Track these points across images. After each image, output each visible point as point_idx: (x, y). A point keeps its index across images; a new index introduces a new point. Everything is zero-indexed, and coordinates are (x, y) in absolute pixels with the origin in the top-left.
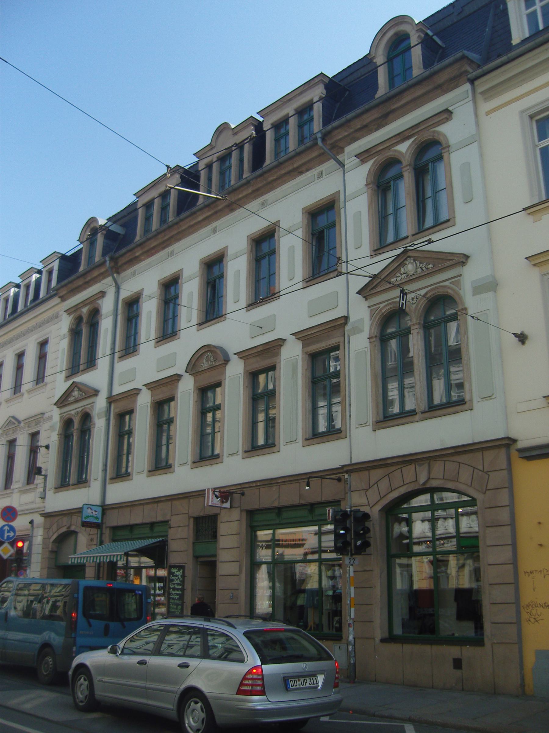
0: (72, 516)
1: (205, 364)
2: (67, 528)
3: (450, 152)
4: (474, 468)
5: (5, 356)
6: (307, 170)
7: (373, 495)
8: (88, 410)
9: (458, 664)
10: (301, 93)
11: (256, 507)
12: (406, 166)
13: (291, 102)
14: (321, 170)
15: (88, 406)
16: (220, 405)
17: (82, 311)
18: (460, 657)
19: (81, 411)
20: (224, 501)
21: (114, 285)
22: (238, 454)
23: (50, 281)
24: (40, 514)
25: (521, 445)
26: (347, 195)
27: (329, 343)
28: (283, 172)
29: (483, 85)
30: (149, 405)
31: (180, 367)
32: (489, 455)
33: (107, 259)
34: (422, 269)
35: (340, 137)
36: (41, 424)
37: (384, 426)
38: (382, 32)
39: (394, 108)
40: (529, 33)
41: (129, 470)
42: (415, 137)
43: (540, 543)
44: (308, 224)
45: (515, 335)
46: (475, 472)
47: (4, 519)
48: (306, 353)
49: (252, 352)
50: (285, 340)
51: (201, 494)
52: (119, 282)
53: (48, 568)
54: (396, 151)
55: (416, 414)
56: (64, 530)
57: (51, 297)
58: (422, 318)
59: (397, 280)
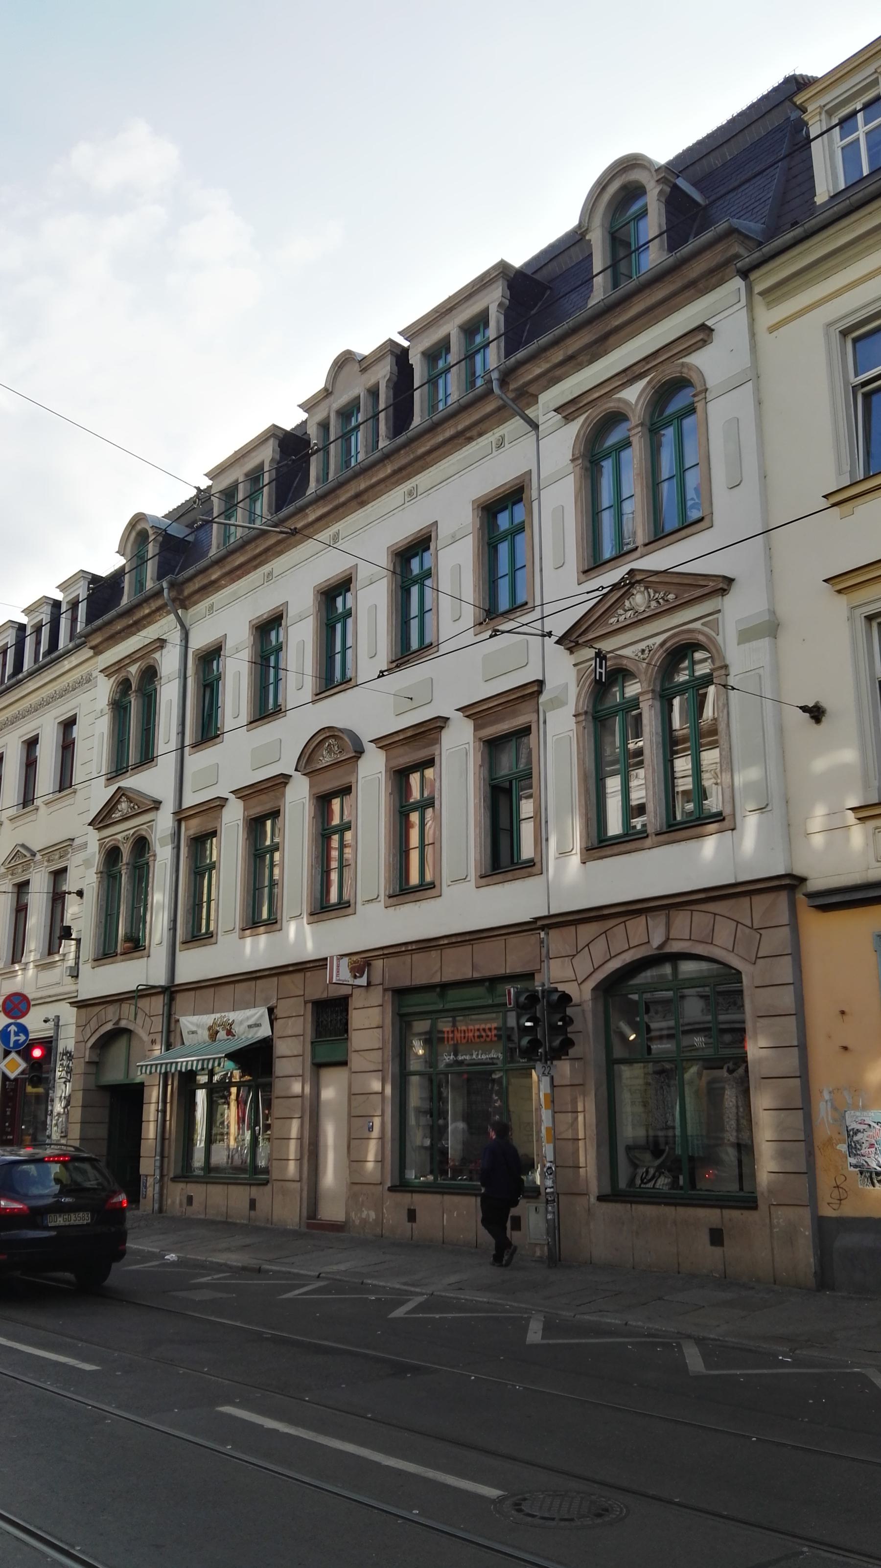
0: (121, 1005)
1: (325, 759)
2: (114, 1024)
3: (707, 400)
4: (738, 922)
5: (5, 745)
6: (480, 435)
7: (583, 966)
8: (144, 833)
9: (717, 1237)
11: (407, 983)
12: (637, 426)
13: (454, 312)
14: (501, 433)
15: (144, 827)
16: (350, 822)
17: (128, 672)
18: (719, 1227)
19: (133, 834)
21: (179, 627)
22: (378, 900)
23: (74, 620)
24: (70, 1003)
25: (814, 885)
26: (542, 477)
27: (515, 724)
28: (440, 438)
29: (764, 280)
30: (241, 823)
31: (287, 766)
32: (761, 902)
33: (165, 585)
34: (658, 602)
35: (530, 377)
36: (69, 856)
37: (598, 855)
38: (601, 186)
39: (617, 323)
40: (588, 566)
41: (212, 928)
42: (652, 375)
43: (844, 1045)
44: (481, 527)
45: (804, 709)
46: (738, 929)
47: (8, 1013)
48: (480, 739)
49: (397, 739)
50: (448, 719)
51: (321, 964)
52: (187, 624)
53: (83, 1090)
54: (620, 400)
55: (647, 836)
56: (109, 1027)
57: (78, 647)
58: (658, 683)
59: (618, 621)
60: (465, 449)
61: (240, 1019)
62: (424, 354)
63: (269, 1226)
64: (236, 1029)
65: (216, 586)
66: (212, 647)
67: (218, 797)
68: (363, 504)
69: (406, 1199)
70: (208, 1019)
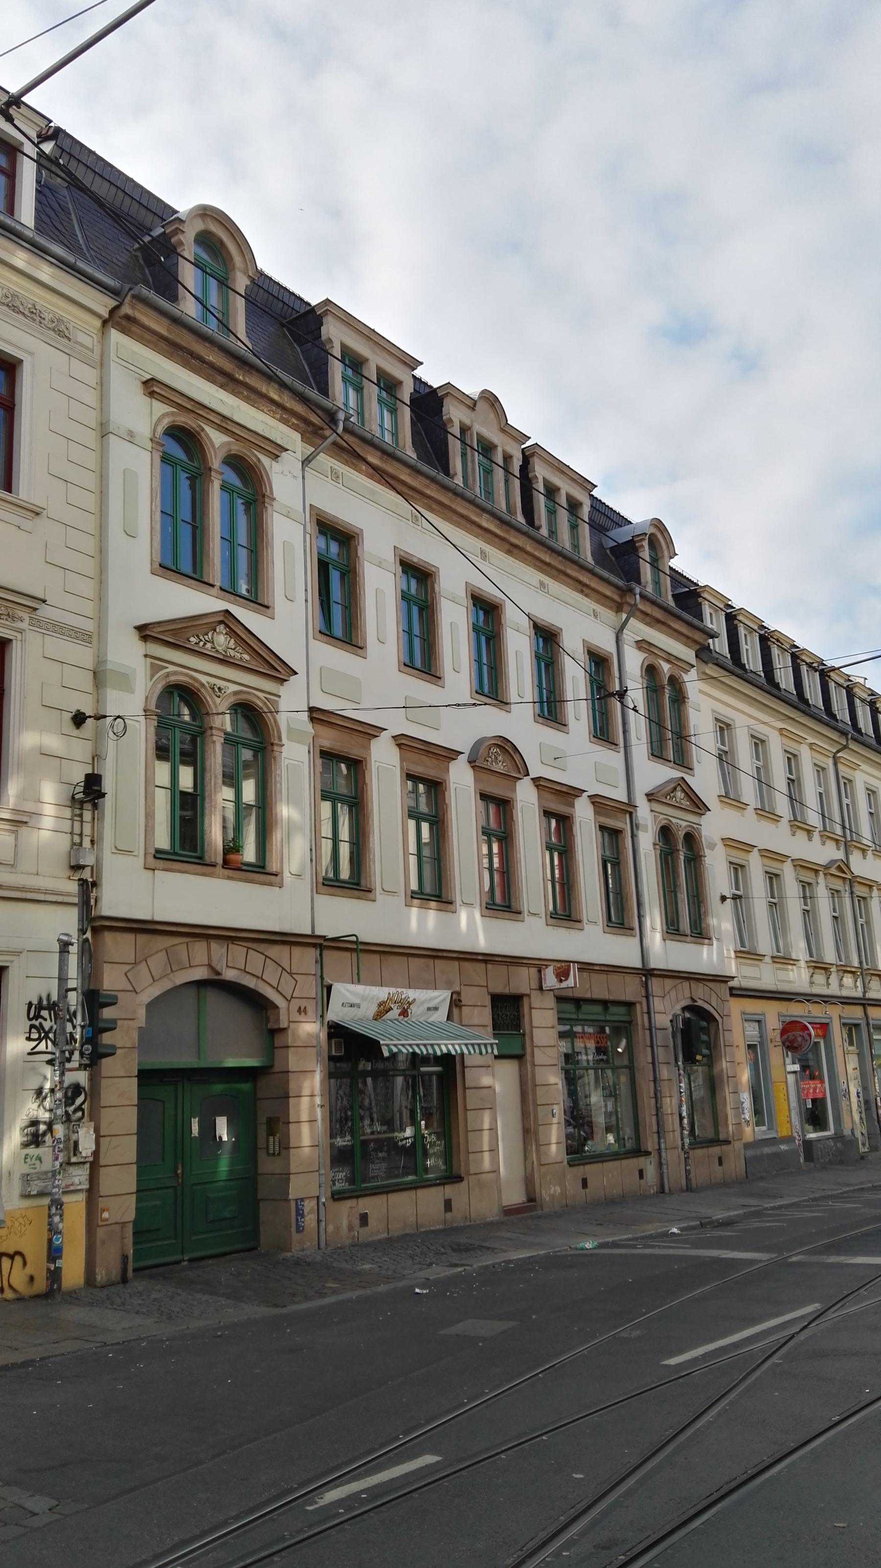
6: (586, 595)
10: (573, 480)
20: (563, 978)
49: (555, 787)
60: (575, 593)
61: (423, 999)
62: (581, 504)
63: (468, 1223)
64: (414, 1010)
65: (354, 461)
66: (342, 526)
67: (403, 735)
68: (509, 552)
69: (580, 1171)
70: (382, 993)
